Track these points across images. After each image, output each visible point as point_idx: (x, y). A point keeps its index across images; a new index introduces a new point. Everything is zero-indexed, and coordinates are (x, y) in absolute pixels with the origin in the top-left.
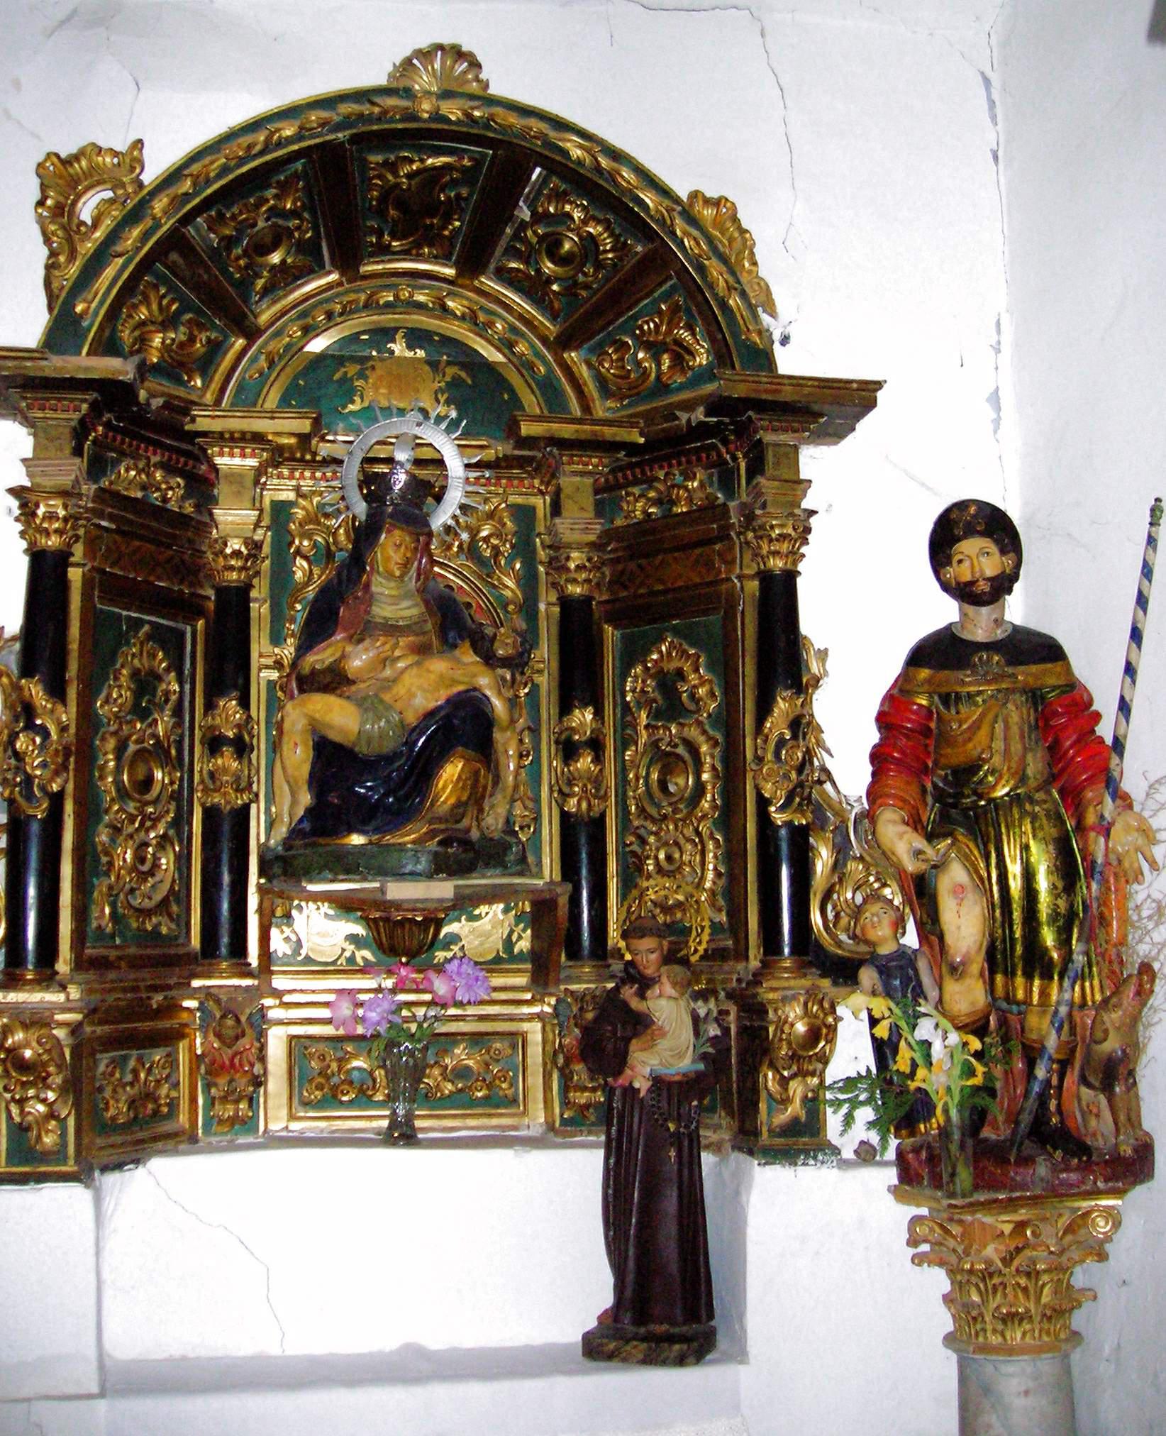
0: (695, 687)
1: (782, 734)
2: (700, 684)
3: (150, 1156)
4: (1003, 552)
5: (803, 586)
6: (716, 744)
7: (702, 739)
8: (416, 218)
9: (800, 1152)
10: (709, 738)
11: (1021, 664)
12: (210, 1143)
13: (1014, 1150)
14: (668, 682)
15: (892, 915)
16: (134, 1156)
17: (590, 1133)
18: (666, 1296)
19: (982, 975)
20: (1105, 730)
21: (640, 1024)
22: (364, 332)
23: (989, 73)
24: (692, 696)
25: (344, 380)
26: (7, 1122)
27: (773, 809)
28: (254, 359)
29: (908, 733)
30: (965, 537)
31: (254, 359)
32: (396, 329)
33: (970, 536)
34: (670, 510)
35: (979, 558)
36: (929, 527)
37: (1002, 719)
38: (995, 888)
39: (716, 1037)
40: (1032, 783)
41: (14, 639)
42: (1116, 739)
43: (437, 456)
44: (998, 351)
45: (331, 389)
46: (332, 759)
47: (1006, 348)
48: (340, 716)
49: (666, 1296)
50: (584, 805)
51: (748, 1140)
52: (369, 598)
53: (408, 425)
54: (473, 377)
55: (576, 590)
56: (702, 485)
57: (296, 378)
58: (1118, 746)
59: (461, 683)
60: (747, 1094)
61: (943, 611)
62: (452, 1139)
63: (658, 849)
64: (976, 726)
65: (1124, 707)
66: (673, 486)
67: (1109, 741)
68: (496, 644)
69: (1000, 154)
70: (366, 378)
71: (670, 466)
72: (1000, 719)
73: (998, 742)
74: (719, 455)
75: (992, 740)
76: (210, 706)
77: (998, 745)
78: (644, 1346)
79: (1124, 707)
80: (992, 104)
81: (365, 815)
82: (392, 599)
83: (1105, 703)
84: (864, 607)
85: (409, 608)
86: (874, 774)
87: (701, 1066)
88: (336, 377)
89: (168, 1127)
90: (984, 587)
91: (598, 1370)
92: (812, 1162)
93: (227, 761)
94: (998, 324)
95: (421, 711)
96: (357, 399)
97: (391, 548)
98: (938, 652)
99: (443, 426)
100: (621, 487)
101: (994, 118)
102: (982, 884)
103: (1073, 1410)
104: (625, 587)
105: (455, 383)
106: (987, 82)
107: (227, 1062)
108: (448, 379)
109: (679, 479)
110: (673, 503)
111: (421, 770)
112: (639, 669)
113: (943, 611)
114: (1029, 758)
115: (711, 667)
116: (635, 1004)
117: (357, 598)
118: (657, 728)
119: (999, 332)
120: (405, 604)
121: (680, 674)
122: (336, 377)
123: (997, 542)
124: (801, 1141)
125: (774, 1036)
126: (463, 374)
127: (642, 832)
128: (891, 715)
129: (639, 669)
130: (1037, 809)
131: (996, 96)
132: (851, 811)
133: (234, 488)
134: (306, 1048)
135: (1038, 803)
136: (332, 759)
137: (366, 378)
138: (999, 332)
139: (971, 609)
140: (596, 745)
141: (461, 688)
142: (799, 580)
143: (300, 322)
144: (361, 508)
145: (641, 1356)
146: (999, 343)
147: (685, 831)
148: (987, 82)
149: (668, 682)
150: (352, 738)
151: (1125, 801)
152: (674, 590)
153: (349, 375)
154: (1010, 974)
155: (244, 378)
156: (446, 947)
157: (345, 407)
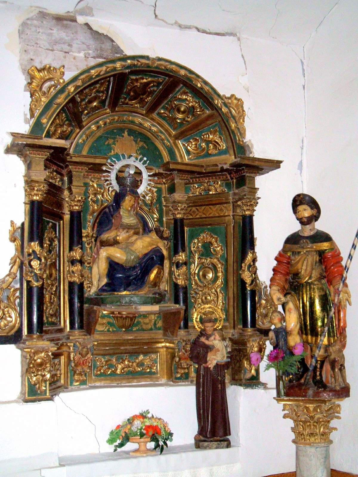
0: (216, 247)
1: (250, 263)
2: (218, 248)
3: (60, 392)
4: (312, 209)
5: (254, 218)
6: (223, 265)
7: (218, 263)
8: (139, 94)
9: (254, 385)
10: (220, 263)
11: (316, 242)
12: (72, 388)
13: (311, 383)
14: (207, 246)
15: (280, 316)
16: (54, 393)
17: (183, 382)
18: (214, 427)
19: (299, 333)
20: (343, 263)
21: (208, 349)
22: (115, 129)
23: (303, 60)
24: (215, 251)
25: (108, 145)
26: (28, 382)
27: (247, 285)
28: (81, 136)
29: (284, 263)
30: (300, 205)
31: (81, 136)
32: (124, 129)
33: (305, 205)
34: (209, 193)
35: (306, 212)
36: (291, 202)
37: (313, 261)
38: (301, 310)
39: (230, 351)
40: (313, 279)
41: (19, 228)
42: (346, 266)
43: (139, 171)
44: (302, 149)
45: (104, 148)
46: (113, 266)
47: (305, 148)
48: (119, 255)
49: (214, 427)
50: (183, 283)
51: (237, 381)
52: (121, 218)
53: (131, 161)
54: (147, 146)
55: (179, 216)
56: (220, 186)
57: (93, 143)
58: (346, 268)
59: (154, 245)
60: (238, 368)
61: (295, 227)
62: (140, 385)
63: (202, 296)
64: (299, 261)
65: (350, 257)
66: (210, 185)
67: (344, 266)
68: (164, 233)
69: (305, 87)
70: (115, 145)
71: (209, 179)
72: (306, 260)
73: (306, 266)
74: (227, 177)
75: (302, 266)
76: (71, 249)
77: (304, 267)
78: (216, 443)
79: (350, 257)
80: (303, 70)
81: (127, 284)
82: (127, 217)
83: (344, 255)
84: (273, 226)
85: (133, 220)
86: (273, 275)
87: (229, 360)
88: (106, 143)
89: (58, 384)
90: (305, 220)
91: (197, 450)
92: (257, 388)
93: (77, 267)
94: (303, 141)
95: (144, 253)
96: (113, 151)
97: (128, 202)
98: (293, 240)
99: (142, 162)
100: (192, 184)
101: (304, 75)
102: (297, 308)
103: (99, 461)
104: (191, 215)
105: (142, 148)
106: (302, 63)
107: (81, 362)
108: (140, 146)
109: (212, 183)
110: (210, 190)
111: (146, 271)
112: (196, 241)
113: (295, 227)
114: (314, 272)
115: (221, 241)
116: (207, 342)
117: (117, 216)
118: (202, 259)
119: (303, 143)
120: (132, 219)
121: (211, 243)
122: (106, 143)
123: (309, 206)
124: (254, 382)
125: (250, 351)
126: (145, 145)
127: (196, 290)
128: (282, 259)
129: (196, 241)
130: (315, 286)
131: (305, 68)
132: (262, 286)
133: (78, 179)
134: (96, 358)
135: (315, 285)
136: (113, 266)
137: (115, 145)
138: (303, 143)
139: (303, 226)
140: (81, 262)
141: (154, 247)
142: (254, 217)
143: (96, 125)
144: (117, 188)
145: (215, 446)
146: (303, 146)
147: (212, 290)
148: (302, 63)
149: (207, 246)
150: (123, 261)
151: (345, 285)
152: (209, 217)
153: (110, 143)
154: (306, 334)
155: (78, 142)
156: (136, 325)
157: (108, 153)
